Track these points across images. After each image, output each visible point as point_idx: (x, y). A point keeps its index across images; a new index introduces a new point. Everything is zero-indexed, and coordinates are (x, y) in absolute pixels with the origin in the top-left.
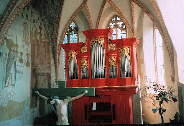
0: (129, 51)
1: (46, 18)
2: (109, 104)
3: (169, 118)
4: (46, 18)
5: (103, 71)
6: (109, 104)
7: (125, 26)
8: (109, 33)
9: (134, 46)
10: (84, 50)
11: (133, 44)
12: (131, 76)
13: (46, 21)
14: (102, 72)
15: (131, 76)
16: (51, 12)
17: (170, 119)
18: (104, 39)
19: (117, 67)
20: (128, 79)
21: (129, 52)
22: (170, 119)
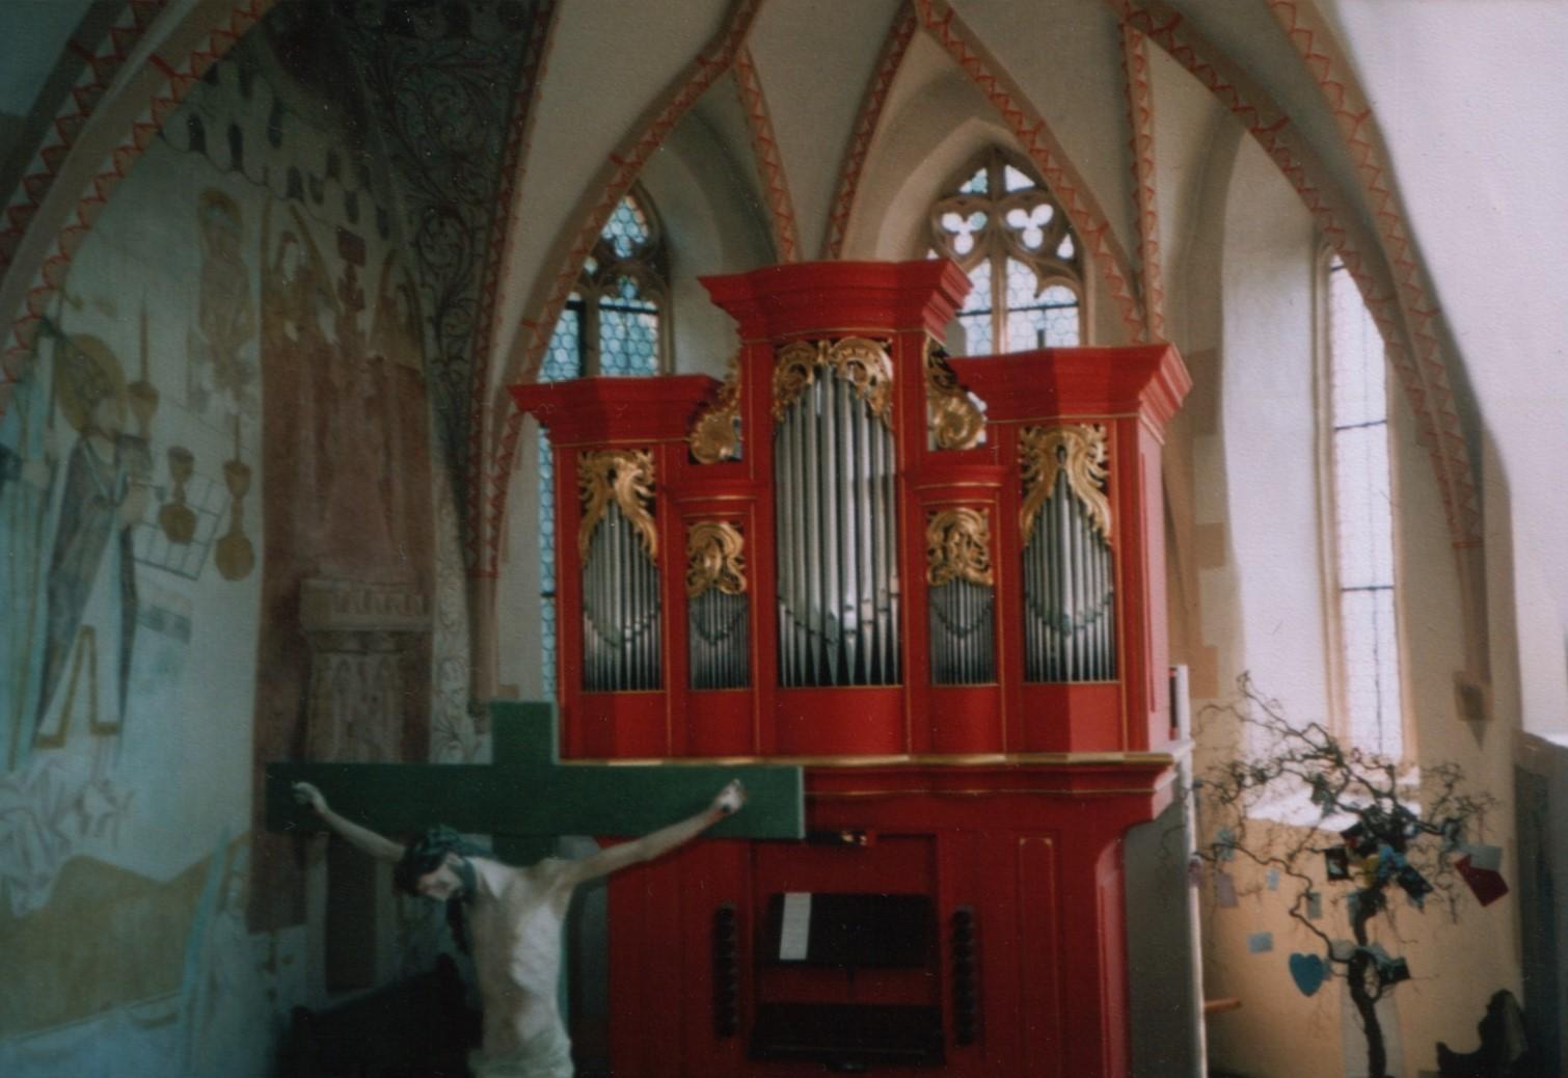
0: (1100, 457)
5: (888, 610)
10: (718, 439)
12: (1115, 674)
15: (1115, 674)
19: (994, 588)
20: (1086, 702)
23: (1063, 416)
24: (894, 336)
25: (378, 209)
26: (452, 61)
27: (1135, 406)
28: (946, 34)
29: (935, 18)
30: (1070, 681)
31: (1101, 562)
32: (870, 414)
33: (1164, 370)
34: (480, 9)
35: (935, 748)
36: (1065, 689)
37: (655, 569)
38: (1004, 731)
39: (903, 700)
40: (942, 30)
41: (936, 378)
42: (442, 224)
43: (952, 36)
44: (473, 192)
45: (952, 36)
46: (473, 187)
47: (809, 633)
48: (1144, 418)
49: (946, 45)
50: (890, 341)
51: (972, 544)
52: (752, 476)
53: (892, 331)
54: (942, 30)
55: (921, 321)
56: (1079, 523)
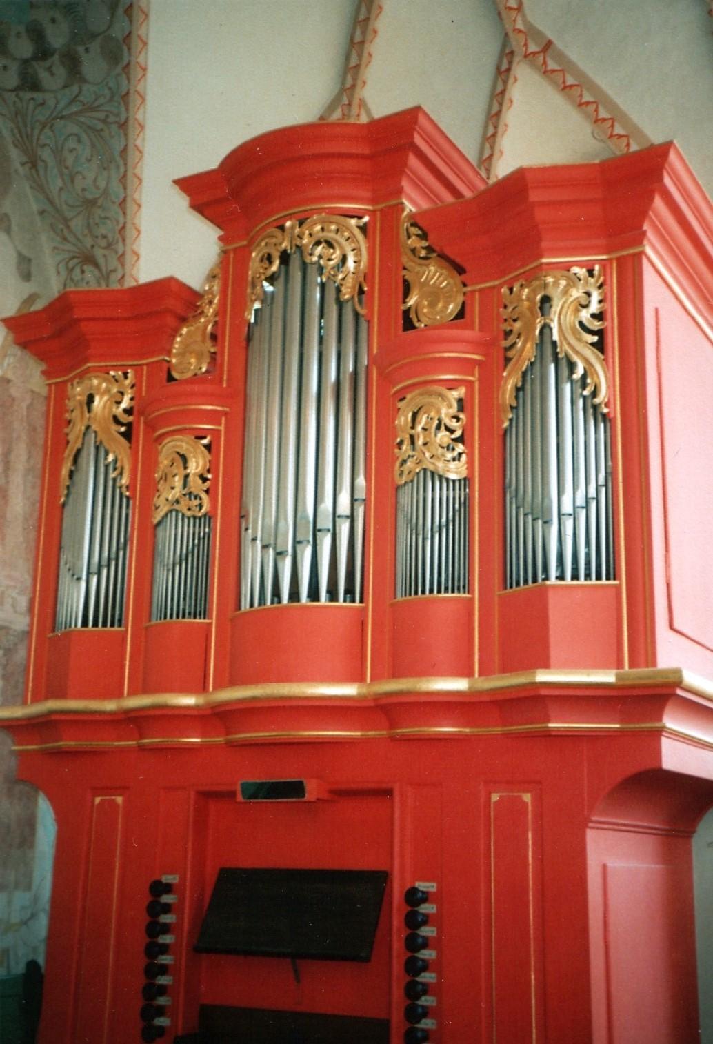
0: (594, 307)
1: (42, 213)
2: (378, 880)
3: (172, 183)
4: (42, 213)
5: (352, 518)
6: (378, 880)
7: (241, 803)
8: (413, 161)
9: (653, 253)
10: (187, 353)
11: (646, 227)
12: (612, 574)
13: (46, 242)
14: (344, 528)
15: (612, 574)
16: (70, 162)
17: (177, 182)
18: (363, 229)
19: (467, 481)
20: (570, 602)
21: (598, 316)
22: (177, 182)
23: (545, 260)
24: (372, 213)
25: (20, 255)
26: (74, 109)
27: (640, 238)
28: (545, 63)
29: (533, 48)
30: (553, 580)
31: (596, 436)
32: (340, 304)
33: (667, 181)
34: (87, 50)
35: (396, 674)
36: (544, 591)
37: (128, 498)
38: (138, 486)
39: (363, 624)
40: (541, 58)
41: (413, 251)
42: (83, 272)
43: (552, 65)
44: (104, 237)
45: (552, 65)
46: (104, 232)
47: (280, 554)
48: (648, 250)
49: (545, 72)
50: (366, 219)
51: (443, 427)
52: (225, 385)
53: (370, 207)
54: (541, 58)
55: (399, 192)
56: (567, 388)
